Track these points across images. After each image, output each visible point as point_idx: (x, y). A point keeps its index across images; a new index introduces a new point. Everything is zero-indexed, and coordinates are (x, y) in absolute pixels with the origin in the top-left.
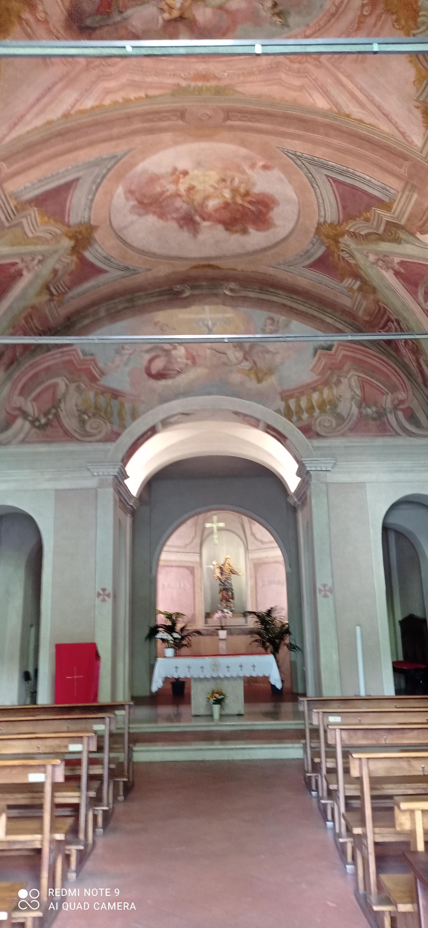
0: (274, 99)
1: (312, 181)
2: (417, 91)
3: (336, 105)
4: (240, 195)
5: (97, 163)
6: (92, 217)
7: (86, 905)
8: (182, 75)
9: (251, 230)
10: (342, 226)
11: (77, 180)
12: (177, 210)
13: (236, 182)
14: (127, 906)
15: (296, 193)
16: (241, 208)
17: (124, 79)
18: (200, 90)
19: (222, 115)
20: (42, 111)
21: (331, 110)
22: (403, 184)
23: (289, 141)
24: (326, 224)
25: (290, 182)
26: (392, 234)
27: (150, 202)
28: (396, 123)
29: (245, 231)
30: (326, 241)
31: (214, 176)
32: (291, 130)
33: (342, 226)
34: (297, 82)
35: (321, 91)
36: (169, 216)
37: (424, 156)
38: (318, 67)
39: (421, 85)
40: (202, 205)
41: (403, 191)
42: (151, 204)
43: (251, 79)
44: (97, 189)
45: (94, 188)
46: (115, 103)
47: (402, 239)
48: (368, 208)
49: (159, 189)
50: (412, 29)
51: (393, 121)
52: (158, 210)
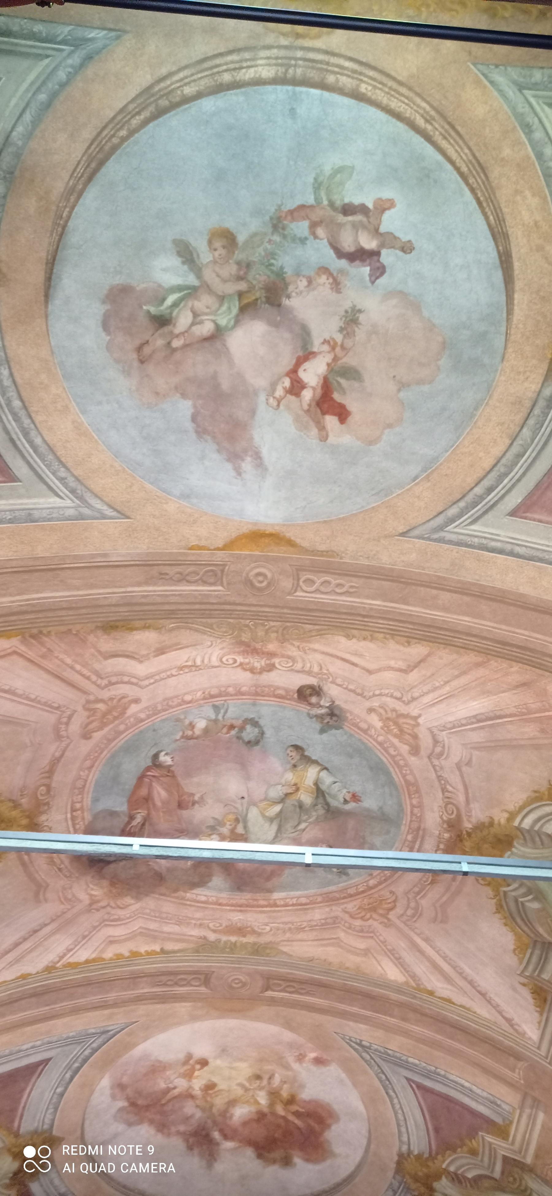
0: (330, 964)
1: (387, 1084)
2: (521, 963)
3: (414, 976)
4: (282, 1101)
5: (78, 1040)
6: (56, 1123)
7: (111, 1166)
8: (211, 925)
9: (297, 1160)
10: (436, 1161)
11: (47, 1061)
12: (187, 1119)
13: (277, 1081)
14: (164, 1168)
15: (363, 1102)
16: (281, 1122)
17: (136, 925)
18: (233, 948)
19: (260, 983)
20: (17, 960)
21: (407, 983)
22: (519, 1097)
23: (351, 1023)
24: (412, 1156)
25: (355, 1085)
26: (515, 1179)
27: (147, 1105)
28: (498, 1006)
29: (287, 1162)
30: (413, 1186)
31: (244, 1070)
32: (355, 1009)
33: (436, 1161)
34: (361, 945)
35: (392, 957)
36: (173, 1129)
37: (543, 1054)
38: (386, 926)
39: (525, 954)
40: (225, 1113)
41: (522, 1107)
42: (147, 1107)
43: (300, 936)
44: (72, 1078)
45: (68, 1076)
46: (119, 956)
47: (531, 1189)
48: (472, 1133)
49: (163, 1085)
50: (501, 886)
51: (493, 1002)
52: (158, 1117)
